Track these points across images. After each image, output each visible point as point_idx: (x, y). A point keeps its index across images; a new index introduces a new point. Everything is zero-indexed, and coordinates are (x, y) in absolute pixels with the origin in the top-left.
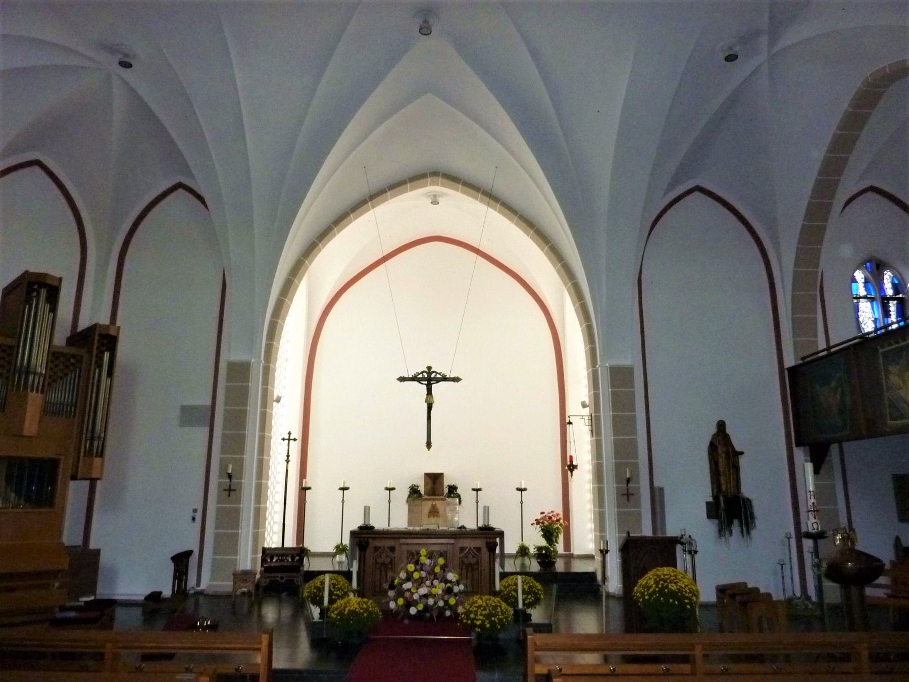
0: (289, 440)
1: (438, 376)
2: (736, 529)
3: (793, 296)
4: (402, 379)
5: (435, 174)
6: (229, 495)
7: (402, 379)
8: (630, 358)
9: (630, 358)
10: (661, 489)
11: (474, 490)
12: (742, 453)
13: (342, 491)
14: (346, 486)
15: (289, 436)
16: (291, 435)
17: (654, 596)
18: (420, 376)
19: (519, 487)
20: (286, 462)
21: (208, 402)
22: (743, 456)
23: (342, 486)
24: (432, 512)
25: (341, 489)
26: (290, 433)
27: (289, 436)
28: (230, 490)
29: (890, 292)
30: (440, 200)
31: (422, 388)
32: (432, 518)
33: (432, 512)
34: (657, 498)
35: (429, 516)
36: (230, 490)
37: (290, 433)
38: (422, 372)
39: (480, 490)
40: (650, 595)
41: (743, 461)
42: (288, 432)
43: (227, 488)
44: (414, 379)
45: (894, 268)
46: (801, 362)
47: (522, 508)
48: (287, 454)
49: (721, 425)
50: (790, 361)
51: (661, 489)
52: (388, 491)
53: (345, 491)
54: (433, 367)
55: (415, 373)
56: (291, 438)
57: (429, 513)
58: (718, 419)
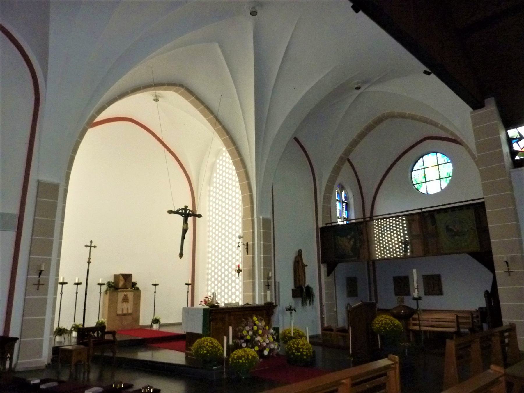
0: (91, 247)
1: (190, 213)
2: (308, 302)
3: (324, 196)
4: (170, 212)
5: (182, 86)
6: (38, 289)
7: (170, 212)
8: (269, 216)
9: (269, 216)
10: (279, 282)
11: (153, 285)
12: (307, 266)
13: (76, 285)
14: (65, 281)
15: (91, 244)
16: (92, 243)
17: (392, 328)
18: (181, 211)
19: (187, 282)
20: (87, 264)
21: (15, 210)
22: (307, 267)
23: (77, 282)
24: (125, 300)
25: (75, 284)
26: (91, 242)
27: (91, 244)
28: (39, 284)
29: (344, 200)
30: (160, 99)
31: (181, 219)
32: (124, 303)
33: (125, 300)
34: (277, 286)
35: (122, 302)
36: (39, 284)
37: (91, 242)
38: (182, 209)
39: (157, 285)
40: (389, 328)
41: (306, 269)
42: (90, 241)
43: (37, 283)
44: (177, 212)
45: (346, 190)
46: (325, 226)
47: (155, 296)
48: (88, 257)
49: (300, 252)
50: (321, 225)
51: (279, 282)
52: (187, 286)
53: (64, 285)
54: (188, 206)
55: (178, 209)
56: (92, 245)
57: (123, 300)
58: (299, 249)
